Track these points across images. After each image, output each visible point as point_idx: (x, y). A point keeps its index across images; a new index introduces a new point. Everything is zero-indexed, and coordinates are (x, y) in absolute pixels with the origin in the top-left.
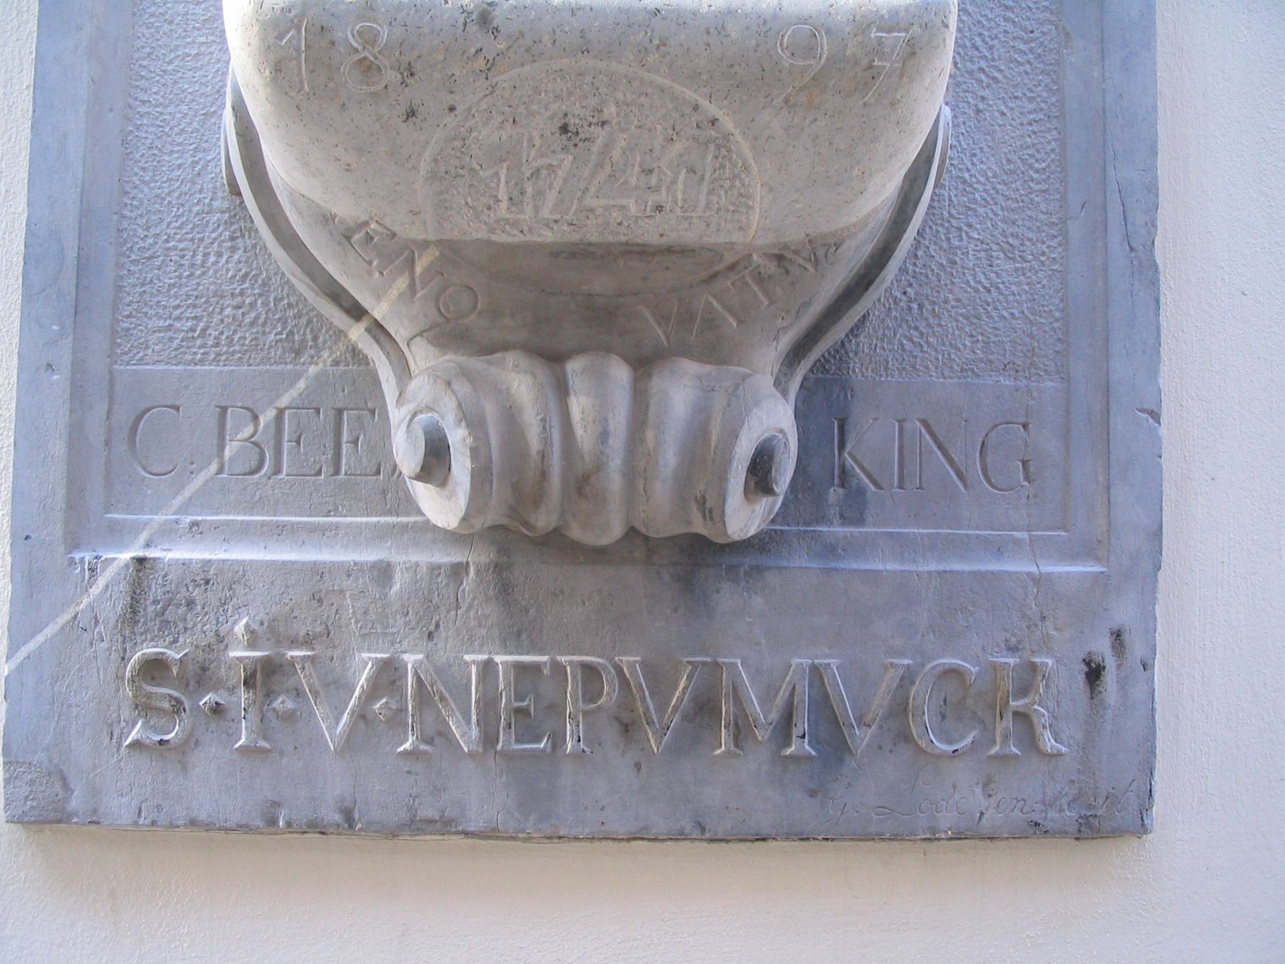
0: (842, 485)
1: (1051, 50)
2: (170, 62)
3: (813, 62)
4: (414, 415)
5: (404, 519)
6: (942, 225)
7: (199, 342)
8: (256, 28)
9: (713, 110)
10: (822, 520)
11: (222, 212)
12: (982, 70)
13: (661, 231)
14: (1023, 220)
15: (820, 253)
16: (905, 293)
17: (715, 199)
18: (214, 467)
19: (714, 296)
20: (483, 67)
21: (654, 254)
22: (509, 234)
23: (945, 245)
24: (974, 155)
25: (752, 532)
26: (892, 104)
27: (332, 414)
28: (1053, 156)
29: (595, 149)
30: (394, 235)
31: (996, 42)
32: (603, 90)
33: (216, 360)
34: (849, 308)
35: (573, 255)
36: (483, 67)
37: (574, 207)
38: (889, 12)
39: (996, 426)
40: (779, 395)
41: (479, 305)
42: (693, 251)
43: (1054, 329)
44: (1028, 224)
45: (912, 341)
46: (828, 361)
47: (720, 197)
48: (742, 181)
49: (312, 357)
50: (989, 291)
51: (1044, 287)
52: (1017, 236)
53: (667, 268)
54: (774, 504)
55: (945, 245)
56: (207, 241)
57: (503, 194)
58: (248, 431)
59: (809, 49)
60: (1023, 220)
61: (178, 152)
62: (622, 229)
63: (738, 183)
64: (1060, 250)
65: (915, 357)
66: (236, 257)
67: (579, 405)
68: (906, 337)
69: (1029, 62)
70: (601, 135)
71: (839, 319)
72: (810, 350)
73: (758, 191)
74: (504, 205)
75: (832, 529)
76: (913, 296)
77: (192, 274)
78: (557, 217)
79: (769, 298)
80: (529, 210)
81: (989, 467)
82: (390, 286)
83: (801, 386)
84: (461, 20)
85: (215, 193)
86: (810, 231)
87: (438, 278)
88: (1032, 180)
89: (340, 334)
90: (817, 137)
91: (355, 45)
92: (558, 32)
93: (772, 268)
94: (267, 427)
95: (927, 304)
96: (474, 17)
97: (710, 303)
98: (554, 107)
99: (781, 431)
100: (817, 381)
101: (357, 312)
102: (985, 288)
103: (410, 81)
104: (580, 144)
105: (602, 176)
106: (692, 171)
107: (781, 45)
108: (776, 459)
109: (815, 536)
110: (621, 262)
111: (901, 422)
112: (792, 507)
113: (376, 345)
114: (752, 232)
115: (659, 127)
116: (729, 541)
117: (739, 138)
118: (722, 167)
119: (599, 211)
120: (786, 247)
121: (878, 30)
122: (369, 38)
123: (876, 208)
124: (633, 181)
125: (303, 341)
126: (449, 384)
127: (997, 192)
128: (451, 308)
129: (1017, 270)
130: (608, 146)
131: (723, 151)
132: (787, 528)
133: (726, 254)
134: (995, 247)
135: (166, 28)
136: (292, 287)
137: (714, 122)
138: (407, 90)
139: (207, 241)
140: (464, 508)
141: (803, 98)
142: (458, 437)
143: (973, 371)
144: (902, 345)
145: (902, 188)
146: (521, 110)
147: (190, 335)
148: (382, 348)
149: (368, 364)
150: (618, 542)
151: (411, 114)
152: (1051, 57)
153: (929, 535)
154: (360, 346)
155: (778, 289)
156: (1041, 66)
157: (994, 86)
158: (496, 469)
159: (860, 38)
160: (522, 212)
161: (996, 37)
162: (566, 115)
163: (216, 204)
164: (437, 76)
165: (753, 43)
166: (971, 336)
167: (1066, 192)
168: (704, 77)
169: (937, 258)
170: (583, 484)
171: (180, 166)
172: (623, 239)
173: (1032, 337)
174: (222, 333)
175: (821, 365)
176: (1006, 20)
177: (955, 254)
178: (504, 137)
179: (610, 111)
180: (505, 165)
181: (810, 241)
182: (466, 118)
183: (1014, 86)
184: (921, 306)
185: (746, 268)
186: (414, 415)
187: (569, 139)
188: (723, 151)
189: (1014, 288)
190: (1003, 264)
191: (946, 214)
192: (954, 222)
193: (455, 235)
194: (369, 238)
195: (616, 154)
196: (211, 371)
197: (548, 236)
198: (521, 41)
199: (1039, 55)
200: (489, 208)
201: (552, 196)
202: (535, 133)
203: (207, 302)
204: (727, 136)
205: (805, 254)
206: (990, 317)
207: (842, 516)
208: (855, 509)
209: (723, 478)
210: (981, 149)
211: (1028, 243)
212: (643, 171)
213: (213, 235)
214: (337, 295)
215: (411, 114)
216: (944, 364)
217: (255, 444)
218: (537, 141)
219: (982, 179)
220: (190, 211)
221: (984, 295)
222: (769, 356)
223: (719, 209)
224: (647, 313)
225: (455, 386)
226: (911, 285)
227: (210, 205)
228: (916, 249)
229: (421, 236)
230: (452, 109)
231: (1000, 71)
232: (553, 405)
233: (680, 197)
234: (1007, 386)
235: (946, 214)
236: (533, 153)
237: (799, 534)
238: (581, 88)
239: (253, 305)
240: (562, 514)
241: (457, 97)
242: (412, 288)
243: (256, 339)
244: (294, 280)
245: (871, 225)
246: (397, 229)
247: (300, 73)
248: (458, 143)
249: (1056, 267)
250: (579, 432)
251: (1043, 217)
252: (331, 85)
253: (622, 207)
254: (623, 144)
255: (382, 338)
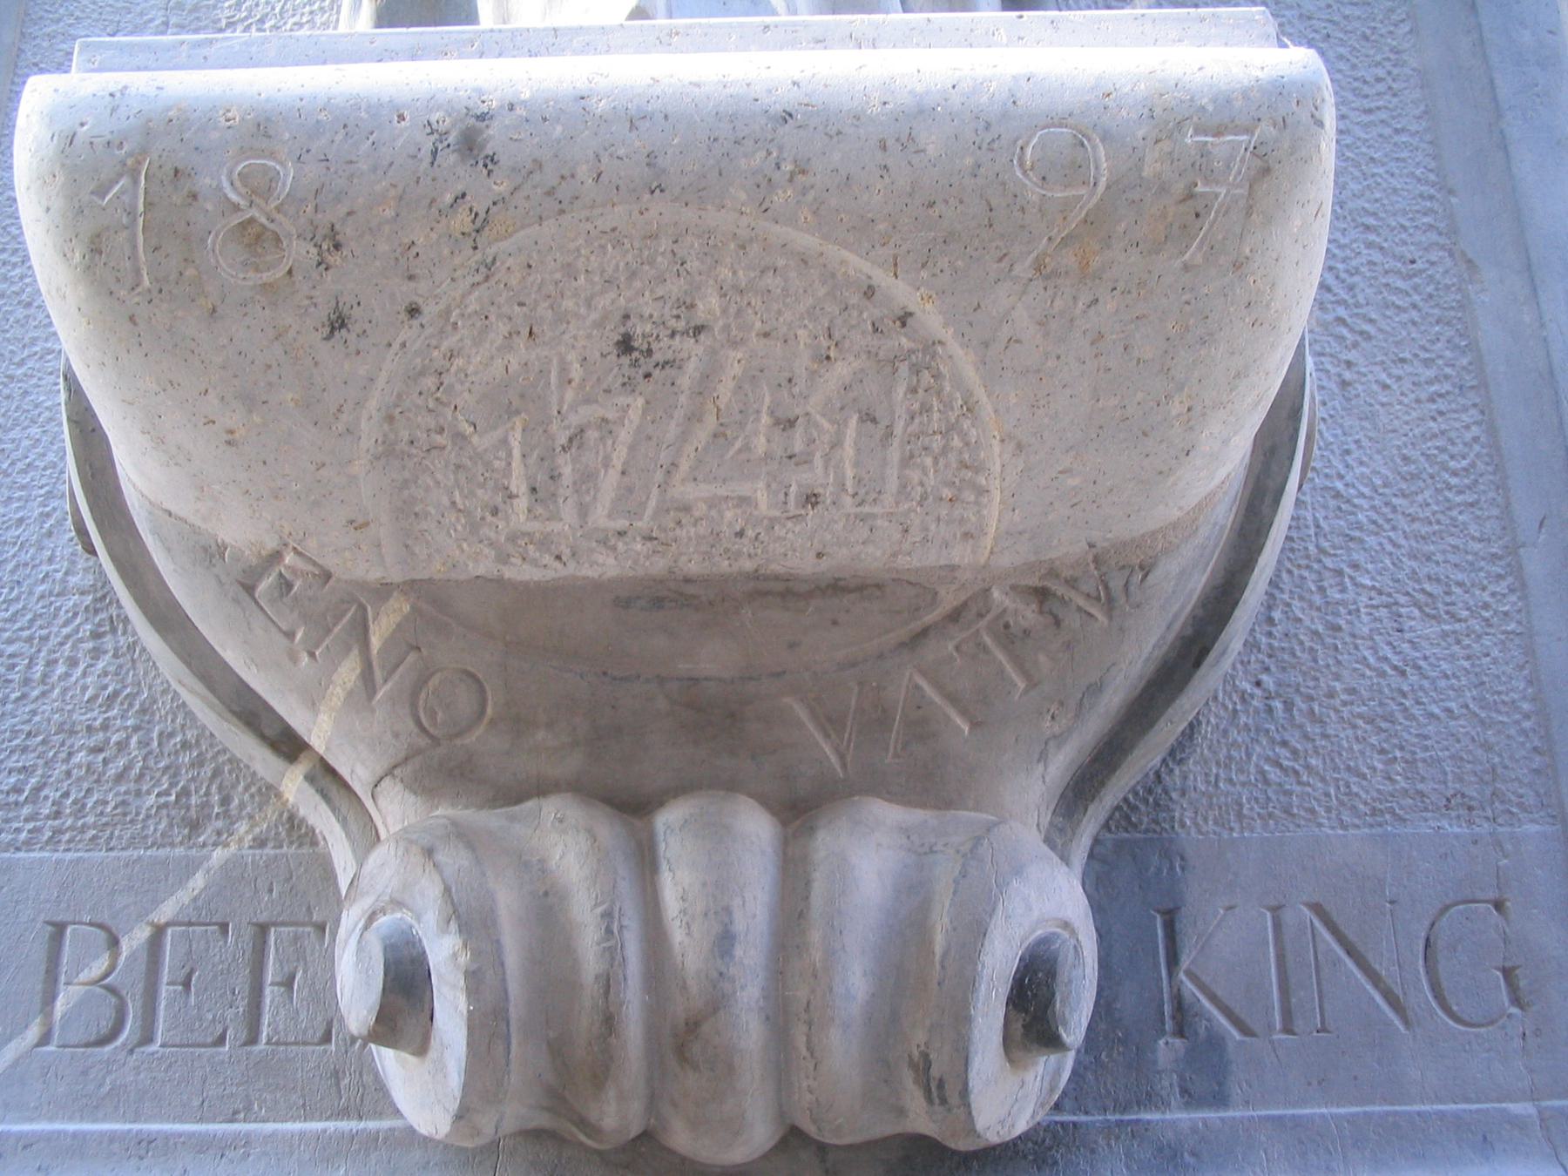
0: (1180, 1032)
1: (1447, 287)
2: (21, 363)
3: (1083, 191)
4: (372, 918)
5: (372, 1125)
6: (1308, 567)
7: (26, 811)
8: (60, 179)
9: (901, 292)
10: (1150, 1099)
11: (82, 593)
12: (1341, 321)
13: (818, 546)
14: (1444, 552)
15: (1116, 584)
16: (1258, 684)
17: (915, 476)
18: (33, 1032)
19: (924, 674)
20: (468, 228)
21: (809, 595)
22: (535, 562)
23: (1317, 599)
24: (1348, 452)
25: (1021, 1126)
26: (1237, 266)
27: (248, 933)
28: (1477, 448)
29: (685, 381)
30: (327, 576)
31: (1356, 279)
32: (693, 265)
33: (53, 841)
34: (1170, 701)
35: (658, 602)
36: (468, 228)
37: (652, 503)
38: (1214, 100)
39: (1446, 908)
40: (1056, 859)
41: (489, 711)
42: (878, 586)
43: (1524, 732)
44: (1452, 558)
45: (1280, 766)
46: (1134, 808)
47: (925, 472)
48: (964, 435)
49: (219, 833)
50: (1403, 673)
51: (1495, 661)
52: (1438, 580)
53: (835, 623)
54: (1058, 1072)
55: (1317, 599)
56: (53, 641)
57: (518, 485)
58: (98, 967)
59: (1076, 171)
60: (1444, 552)
61: (19, 499)
62: (745, 545)
63: (956, 442)
64: (1513, 598)
65: (1288, 793)
66: (101, 665)
67: (678, 885)
68: (1268, 759)
69: (1414, 306)
70: (693, 352)
71: (1152, 724)
72: (1102, 784)
73: (995, 454)
74: (522, 503)
75: (1168, 1116)
76: (1272, 687)
77: (24, 696)
78: (621, 524)
79: (1026, 675)
80: (568, 512)
81: (1445, 984)
82: (330, 682)
83: (1091, 856)
84: (430, 146)
85: (73, 563)
86: (1096, 536)
87: (412, 657)
88: (1450, 488)
89: (269, 792)
90: (1101, 336)
91: (234, 197)
92: (605, 159)
93: (1028, 615)
94: (133, 957)
95: (1298, 700)
96: (451, 139)
97: (917, 687)
98: (603, 302)
99: (1066, 925)
100: (1119, 846)
101: (289, 745)
102: (1395, 668)
103: (334, 259)
104: (656, 373)
105: (702, 435)
106: (869, 418)
107: (1021, 163)
108: (1062, 977)
109: (1138, 1131)
110: (747, 612)
111: (1276, 910)
112: (1090, 1076)
113: (323, 807)
114: (988, 542)
115: (800, 332)
116: (981, 1144)
117: (954, 347)
118: (926, 409)
119: (700, 509)
120: (1052, 573)
121: (1197, 132)
122: (259, 186)
123: (1212, 494)
124: (760, 445)
125: (205, 805)
126: (429, 852)
127: (1394, 510)
128: (440, 715)
129: (1444, 635)
130: (707, 378)
131: (926, 376)
132: (1083, 1118)
133: (942, 592)
134: (1403, 599)
135: (21, 313)
136: (189, 715)
137: (904, 319)
138: (329, 276)
139: (53, 641)
140: (458, 1094)
141: (1069, 259)
142: (444, 953)
143: (1393, 813)
144: (1262, 773)
145: (1250, 467)
146: (543, 309)
147: (12, 798)
148: (334, 810)
149: (314, 843)
150: (765, 1157)
151: (338, 323)
152: (1452, 298)
153: (1352, 1119)
154: (302, 812)
155: (1042, 658)
156: (1436, 311)
157: (1364, 344)
158: (516, 1011)
159: (1166, 146)
160: (555, 517)
161: (1357, 271)
162: (627, 317)
163: (73, 580)
164: (383, 247)
165: (969, 161)
166: (1382, 751)
167: (1508, 504)
168: (882, 227)
169: (1307, 623)
170: (686, 1039)
171: (21, 520)
172: (748, 565)
173: (1487, 747)
174: (66, 795)
175: (1123, 816)
176: (1369, 245)
177: (1336, 614)
178: (514, 367)
179: (709, 305)
180: (518, 422)
181: (1096, 560)
182: (442, 331)
183: (1397, 344)
184: (1289, 706)
185: (980, 616)
186: (372, 918)
187: (635, 364)
188: (926, 376)
189: (1444, 665)
190: (1416, 624)
191: (1311, 548)
192: (1328, 562)
193: (436, 569)
194: (285, 585)
195: (725, 391)
196: (42, 861)
197: (606, 566)
198: (537, 177)
199: (1431, 296)
200: (495, 512)
201: (609, 482)
202: (572, 357)
203: (44, 742)
204: (931, 346)
205: (1088, 586)
206: (1412, 718)
207: (1184, 1091)
208: (1207, 1077)
209: (961, 1019)
210: (1357, 442)
211: (1458, 590)
212: (777, 422)
213: (65, 631)
214: (252, 713)
215: (338, 323)
216: (1342, 803)
217: (112, 990)
218: (576, 372)
219: (1366, 491)
220: (31, 593)
221: (1395, 681)
222: (1031, 790)
223: (924, 497)
224: (801, 713)
225: (440, 857)
226: (1267, 669)
227: (64, 581)
228: (1270, 608)
229: (375, 575)
230: (413, 311)
231: (1371, 321)
232: (627, 889)
233: (850, 473)
234: (1457, 836)
235: (1311, 548)
236: (570, 395)
237: (1108, 1130)
238: (651, 262)
239: (122, 746)
240: (652, 1100)
241: (423, 286)
242: (367, 676)
243: (124, 803)
244: (185, 695)
245: (1204, 531)
246: (330, 562)
247: (133, 256)
248: (429, 382)
249: (1512, 626)
250: (678, 936)
251: (1477, 546)
252: (190, 272)
253: (743, 501)
254: (737, 370)
255: (334, 791)
